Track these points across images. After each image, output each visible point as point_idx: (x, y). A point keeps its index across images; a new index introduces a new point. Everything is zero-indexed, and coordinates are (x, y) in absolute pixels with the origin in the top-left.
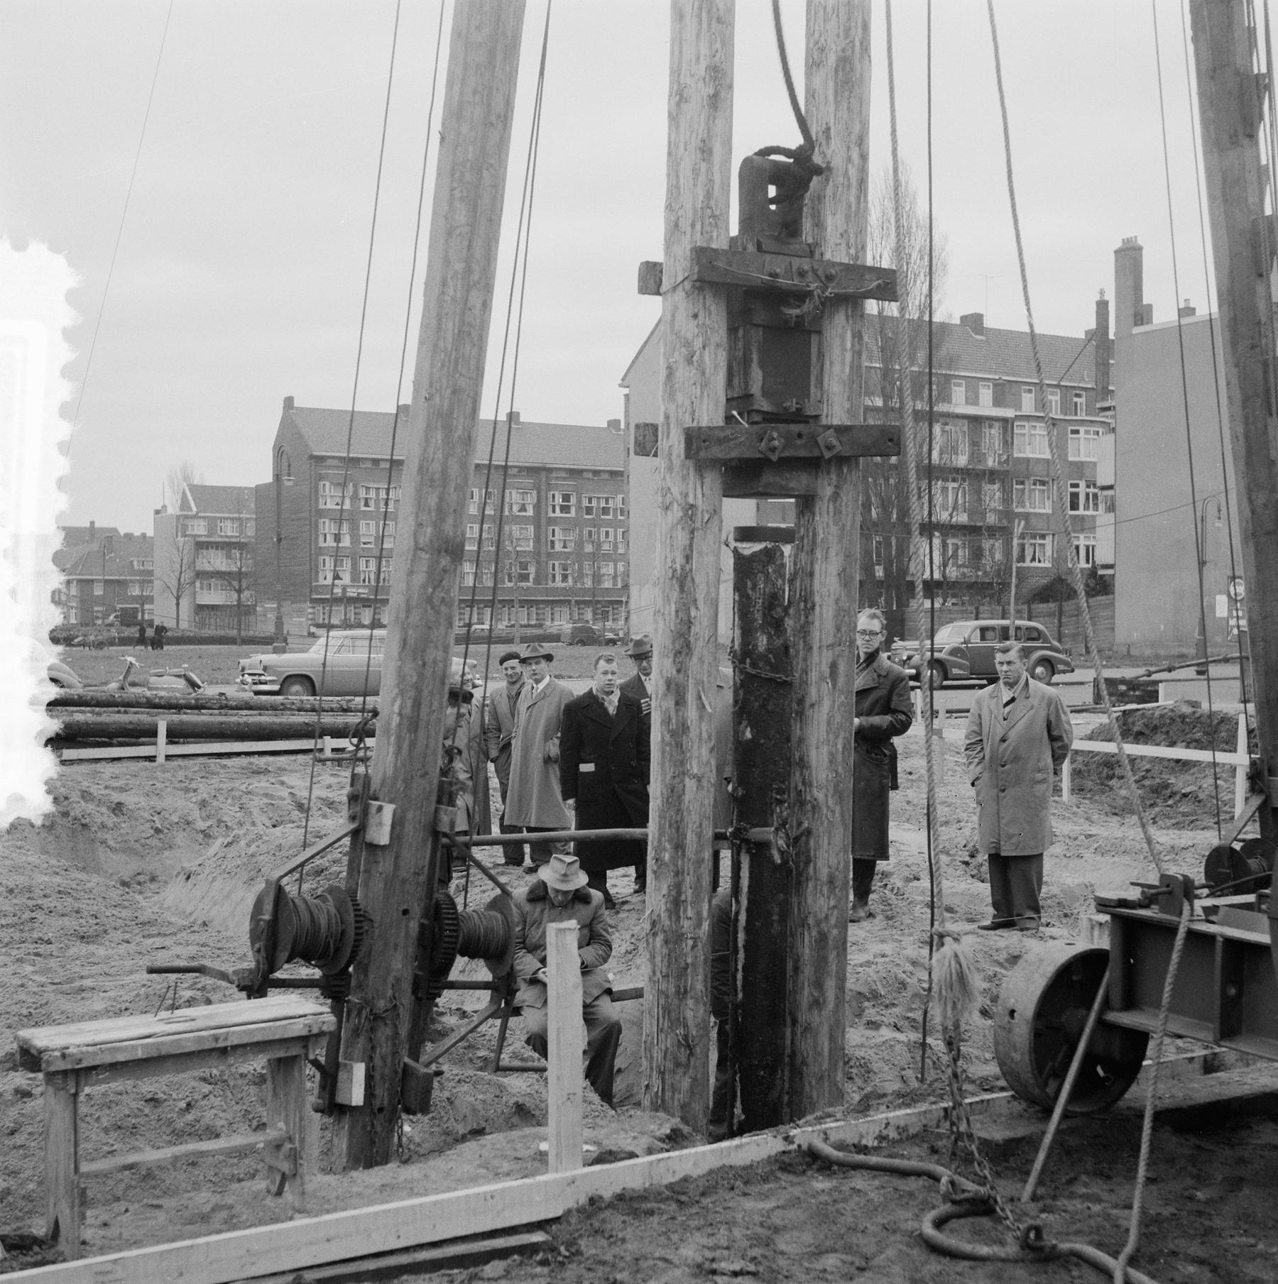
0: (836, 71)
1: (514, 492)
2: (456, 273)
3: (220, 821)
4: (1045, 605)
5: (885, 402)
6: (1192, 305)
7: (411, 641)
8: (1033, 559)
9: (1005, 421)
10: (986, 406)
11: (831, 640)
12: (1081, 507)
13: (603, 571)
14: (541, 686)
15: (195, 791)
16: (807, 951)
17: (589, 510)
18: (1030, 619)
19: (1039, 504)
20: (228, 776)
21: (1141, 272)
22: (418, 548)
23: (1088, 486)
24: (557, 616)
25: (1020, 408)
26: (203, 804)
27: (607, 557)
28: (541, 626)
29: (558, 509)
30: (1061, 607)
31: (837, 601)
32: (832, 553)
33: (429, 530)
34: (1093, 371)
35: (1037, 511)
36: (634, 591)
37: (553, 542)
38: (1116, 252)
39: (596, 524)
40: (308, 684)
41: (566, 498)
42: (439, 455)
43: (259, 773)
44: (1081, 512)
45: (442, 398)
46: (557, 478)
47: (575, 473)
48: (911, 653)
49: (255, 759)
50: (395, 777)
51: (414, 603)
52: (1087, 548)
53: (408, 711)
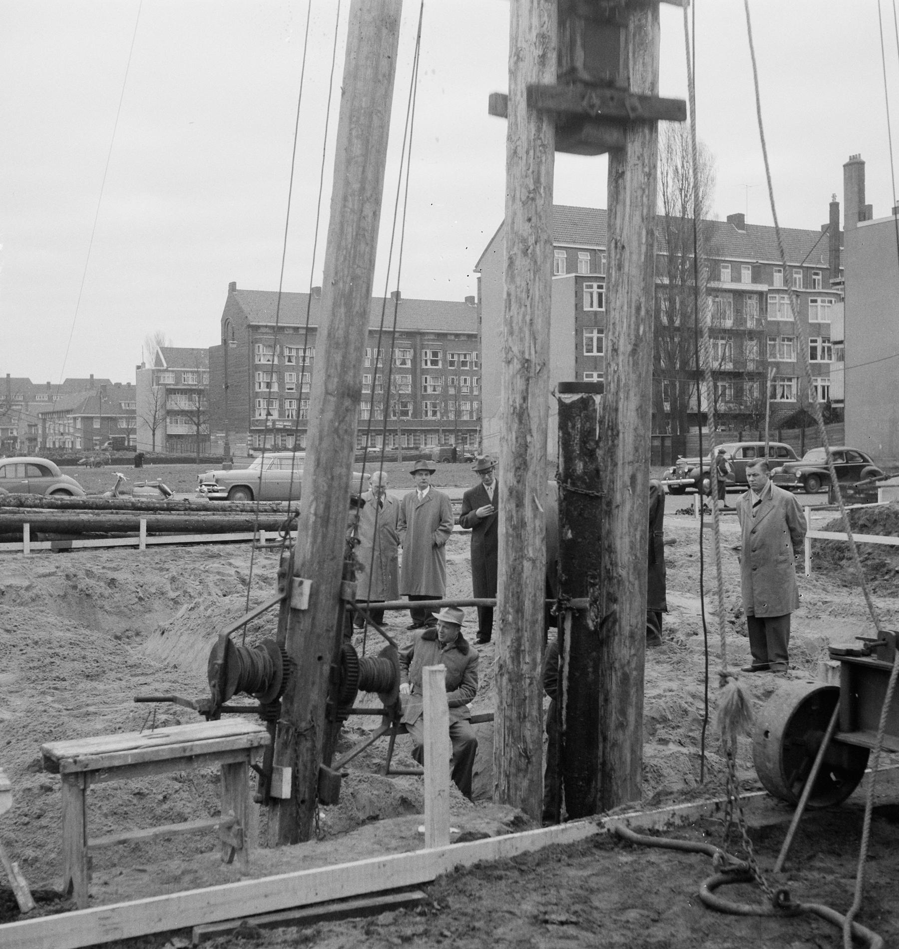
3: (185, 592)
4: (791, 431)
7: (323, 460)
8: (783, 397)
9: (761, 294)
10: (746, 283)
11: (631, 458)
12: (819, 357)
13: (463, 408)
14: (426, 492)
17: (452, 363)
19: (787, 355)
22: (327, 393)
23: (824, 342)
24: (429, 441)
26: (173, 580)
27: (466, 398)
28: (417, 448)
29: (429, 363)
31: (636, 429)
32: (632, 394)
35: (785, 360)
36: (485, 423)
37: (425, 387)
38: (844, 166)
39: (457, 373)
40: (249, 493)
41: (435, 354)
42: (343, 325)
44: (819, 360)
46: (428, 340)
47: (441, 336)
52: (823, 387)
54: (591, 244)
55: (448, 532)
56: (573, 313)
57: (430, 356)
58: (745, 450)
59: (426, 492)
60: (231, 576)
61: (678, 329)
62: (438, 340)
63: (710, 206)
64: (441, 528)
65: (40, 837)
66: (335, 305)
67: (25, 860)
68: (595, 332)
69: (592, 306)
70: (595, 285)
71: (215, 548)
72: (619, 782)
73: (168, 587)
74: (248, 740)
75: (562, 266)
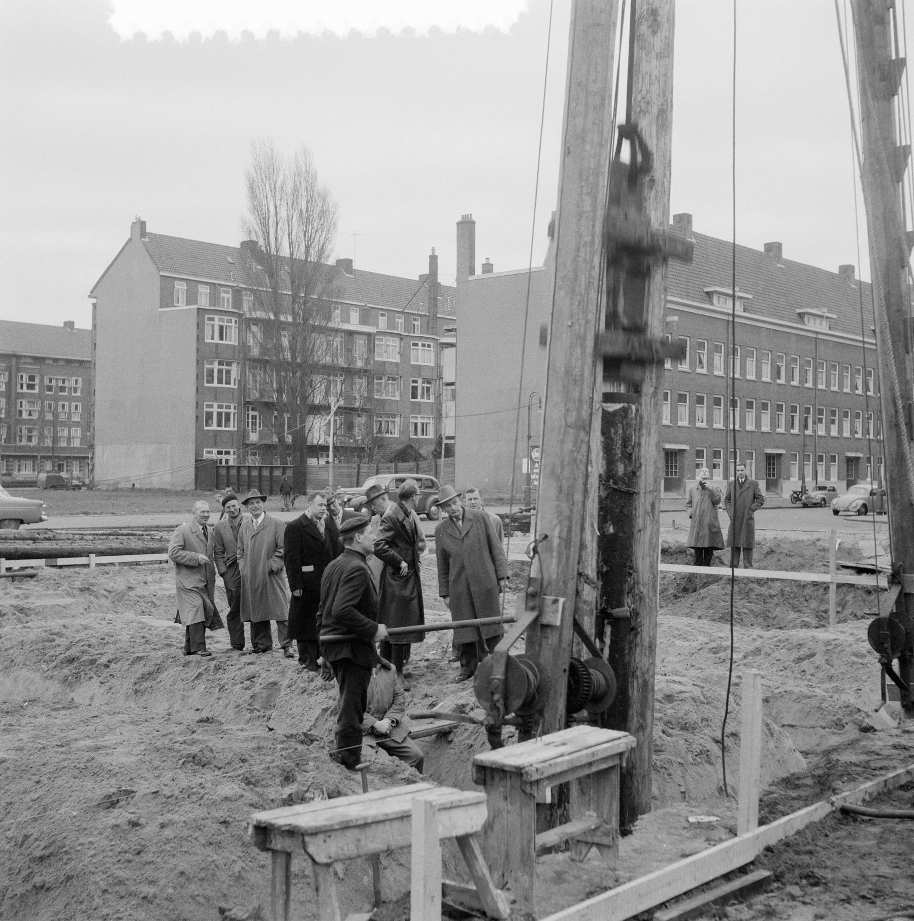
0: (658, 117)
2: (586, 243)
4: (406, 464)
7: (565, 488)
8: (387, 432)
9: (369, 335)
10: (354, 324)
11: (651, 488)
12: (419, 396)
14: (260, 520)
16: (636, 692)
18: (396, 472)
19: (391, 393)
21: (474, 239)
22: (567, 426)
23: (424, 383)
24: (23, 467)
27: (63, 424)
29: (25, 386)
30: (418, 465)
32: (653, 431)
33: (574, 413)
34: (426, 306)
36: (98, 450)
37: (20, 412)
38: (458, 224)
39: (56, 399)
41: (32, 378)
44: (419, 400)
46: (25, 363)
48: (351, 496)
52: (423, 424)
53: (564, 534)
54: (211, 278)
57: (26, 380)
61: (300, 365)
62: (35, 364)
63: (332, 250)
65: (149, 871)
67: (144, 898)
68: (216, 363)
70: (217, 318)
74: (627, 744)
75: (182, 298)
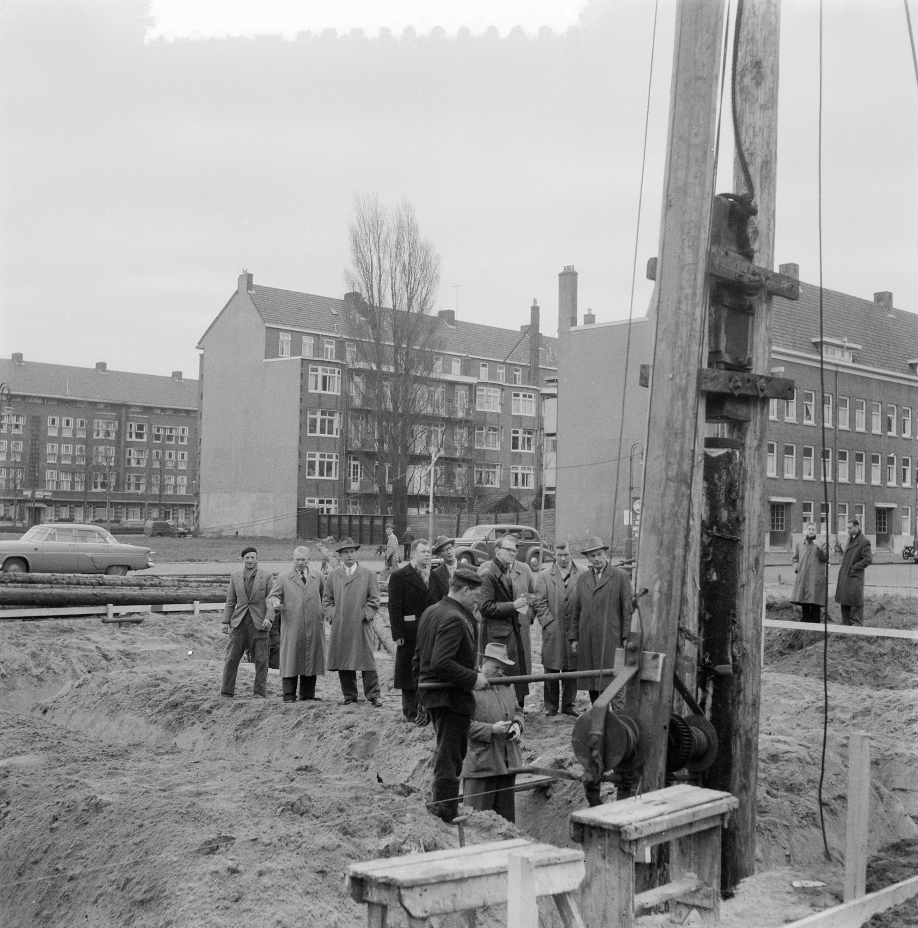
0: (762, 170)
1: (101, 421)
3: (49, 668)
4: (506, 515)
5: (396, 369)
6: (593, 313)
8: (487, 482)
9: (470, 386)
10: (455, 375)
11: (755, 542)
12: (520, 447)
13: (166, 482)
15: (24, 645)
16: (738, 751)
17: (157, 437)
18: (496, 523)
19: (492, 444)
20: (39, 636)
21: (576, 290)
22: (668, 479)
23: (524, 433)
24: (131, 514)
25: (479, 377)
26: (33, 655)
27: (170, 472)
28: (118, 522)
29: (134, 435)
31: (760, 516)
32: (757, 484)
34: (528, 357)
35: (490, 448)
36: (203, 497)
37: (129, 460)
39: (163, 448)
40: (23, 564)
41: (140, 427)
42: (680, 417)
43: (66, 632)
44: (520, 450)
45: (681, 379)
46: (134, 413)
47: (147, 409)
49: (59, 621)
50: (658, 634)
51: (667, 516)
52: (523, 475)
53: (665, 589)
54: (315, 329)
55: (375, 608)
56: (297, 396)
58: (498, 531)
59: (354, 568)
60: (92, 651)
61: (402, 415)
63: (434, 302)
64: (369, 603)
66: (673, 399)
68: (319, 413)
69: (316, 388)
71: (65, 622)
72: (742, 840)
73: (31, 663)
75: (287, 348)
